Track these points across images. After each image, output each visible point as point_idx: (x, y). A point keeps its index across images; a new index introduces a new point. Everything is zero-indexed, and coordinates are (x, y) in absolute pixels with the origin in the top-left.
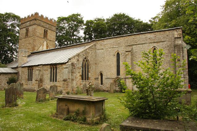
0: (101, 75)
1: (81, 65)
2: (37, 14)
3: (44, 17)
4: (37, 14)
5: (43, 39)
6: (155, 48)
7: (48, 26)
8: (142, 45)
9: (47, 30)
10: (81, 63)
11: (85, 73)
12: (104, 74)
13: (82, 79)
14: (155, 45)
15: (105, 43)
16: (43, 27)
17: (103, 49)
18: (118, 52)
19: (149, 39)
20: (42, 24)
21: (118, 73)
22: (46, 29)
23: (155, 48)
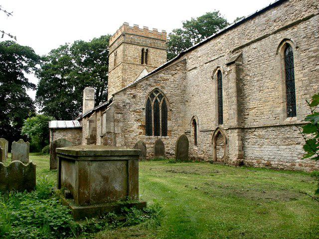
0: (195, 124)
1: (142, 105)
2: (126, 25)
3: (141, 27)
4: (126, 25)
5: (141, 67)
6: (288, 42)
7: (149, 41)
8: (259, 43)
9: (147, 50)
10: (144, 101)
11: (156, 117)
12: (199, 121)
13: (148, 133)
14: (287, 34)
15: (199, 54)
16: (138, 44)
17: (195, 68)
18: (218, 69)
19: (275, 21)
20: (137, 39)
21: (221, 121)
22: (145, 48)
23: (288, 42)
